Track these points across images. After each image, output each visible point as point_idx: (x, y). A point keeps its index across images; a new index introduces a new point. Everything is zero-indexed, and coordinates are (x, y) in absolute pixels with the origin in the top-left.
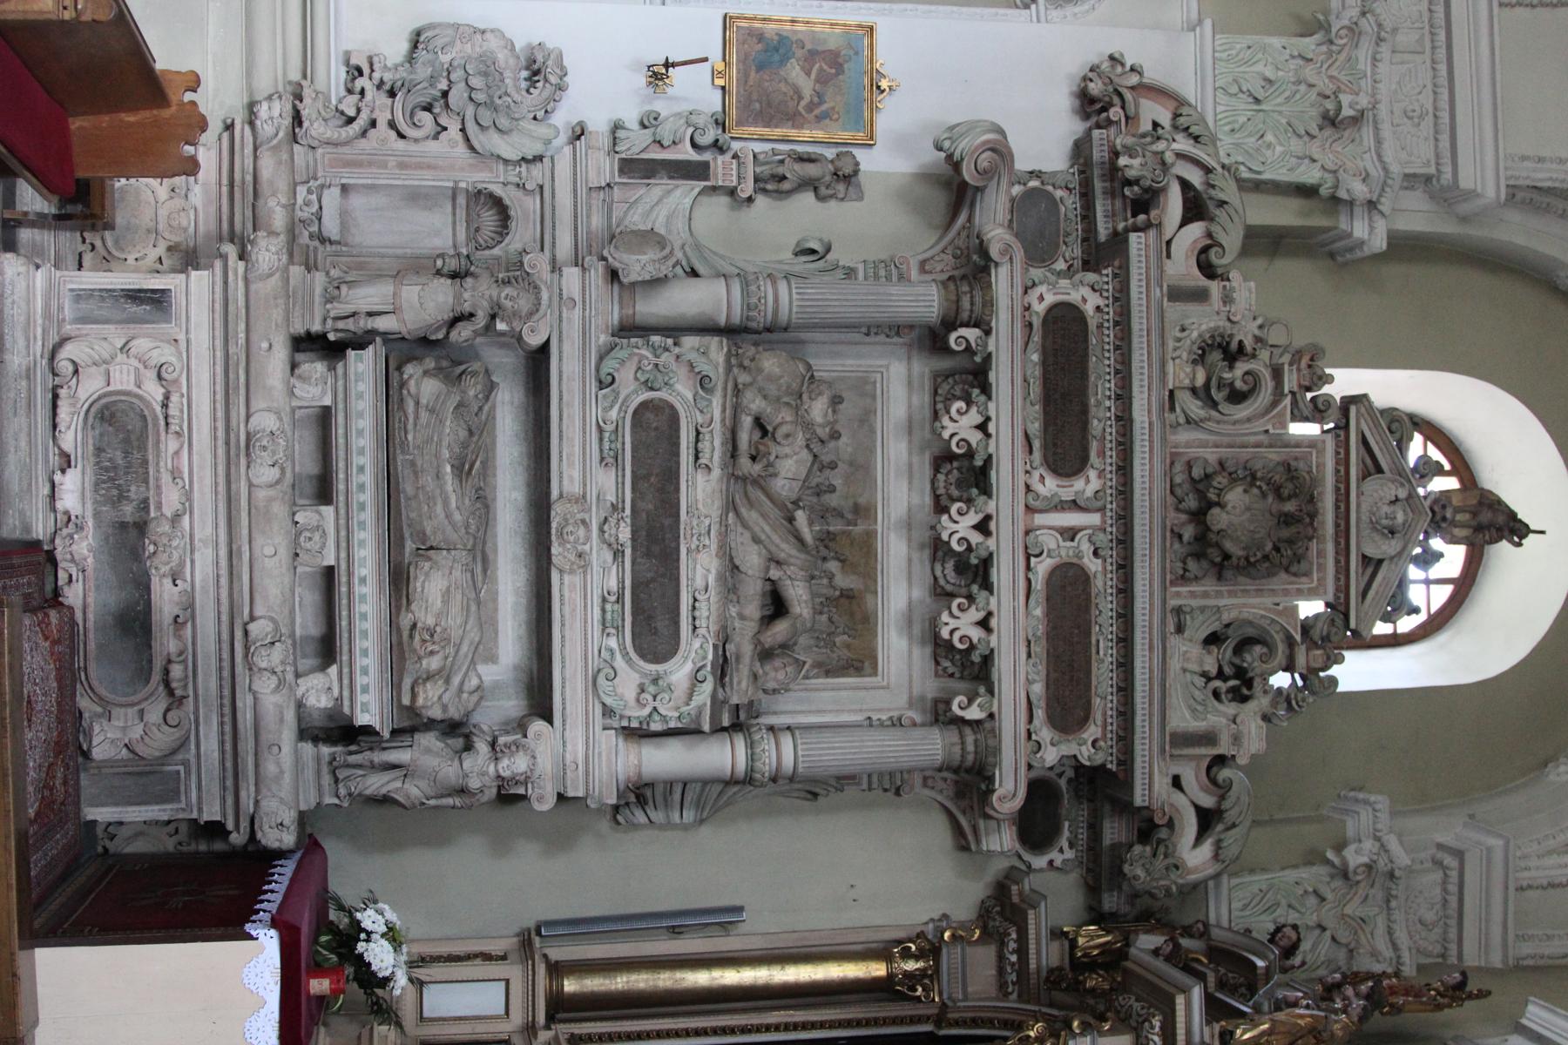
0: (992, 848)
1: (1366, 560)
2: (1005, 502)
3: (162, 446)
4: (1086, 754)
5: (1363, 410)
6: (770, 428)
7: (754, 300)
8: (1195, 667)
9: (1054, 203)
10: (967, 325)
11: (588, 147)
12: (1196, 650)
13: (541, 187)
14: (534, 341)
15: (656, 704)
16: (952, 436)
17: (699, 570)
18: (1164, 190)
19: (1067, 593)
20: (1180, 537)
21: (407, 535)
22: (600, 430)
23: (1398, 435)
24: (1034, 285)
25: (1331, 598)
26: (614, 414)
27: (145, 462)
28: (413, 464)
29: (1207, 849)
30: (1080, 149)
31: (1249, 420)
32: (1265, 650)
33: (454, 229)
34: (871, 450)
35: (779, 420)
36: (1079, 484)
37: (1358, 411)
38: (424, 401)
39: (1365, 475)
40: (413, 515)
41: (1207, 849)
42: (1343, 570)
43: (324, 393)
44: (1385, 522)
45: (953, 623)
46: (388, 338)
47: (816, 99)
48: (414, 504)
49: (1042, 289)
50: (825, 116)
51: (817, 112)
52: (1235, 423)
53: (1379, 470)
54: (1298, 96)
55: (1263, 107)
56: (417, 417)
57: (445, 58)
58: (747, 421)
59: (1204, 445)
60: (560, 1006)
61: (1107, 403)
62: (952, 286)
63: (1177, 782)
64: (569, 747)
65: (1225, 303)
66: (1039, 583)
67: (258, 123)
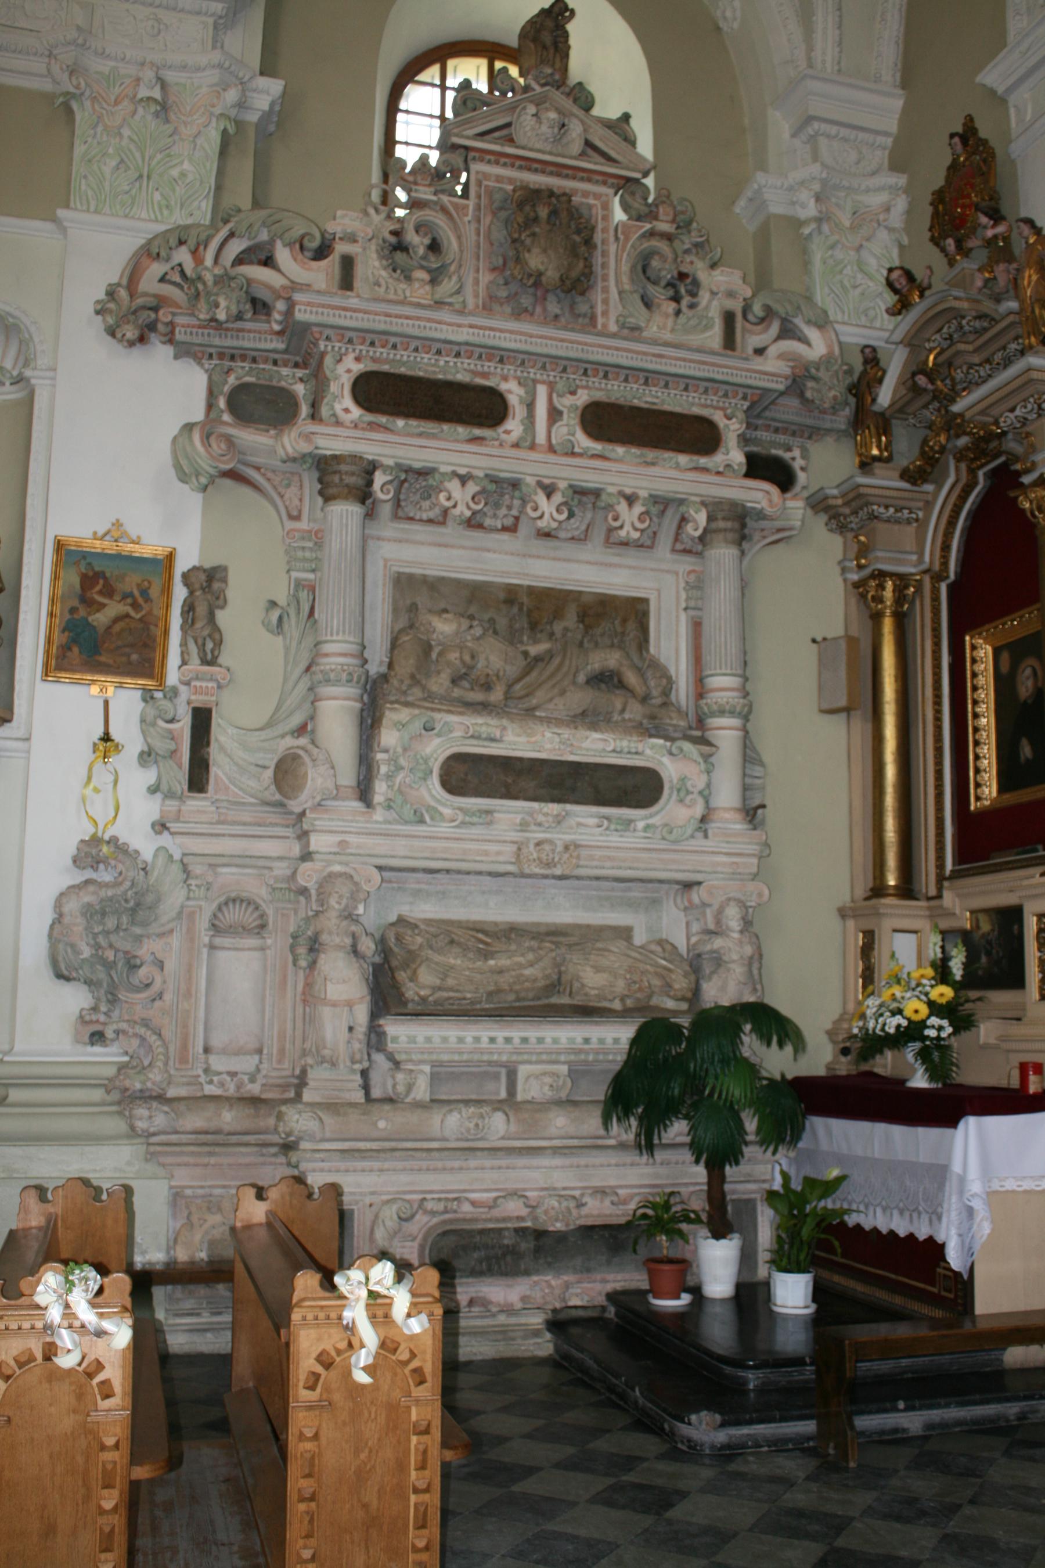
0: (800, 517)
1: (583, 154)
2: (530, 467)
3: (469, 1216)
4: (737, 426)
5: (455, 131)
6: (463, 671)
7: (344, 676)
8: (670, 322)
9: (242, 389)
10: (370, 483)
11: (177, 820)
12: (657, 319)
13: (210, 865)
14: (376, 876)
15: (696, 791)
16: (469, 508)
17: (596, 747)
18: (249, 282)
19: (607, 422)
20: (556, 316)
21: (545, 1001)
22: (463, 824)
23: (478, 104)
24: (334, 415)
25: (611, 191)
26: (447, 811)
27: (482, 1232)
28: (490, 994)
29: (813, 334)
30: (184, 351)
31: (459, 237)
32: (656, 257)
33: (243, 949)
34: (458, 582)
35: (457, 662)
36: (513, 400)
37: (457, 135)
38: (438, 982)
39: (511, 140)
40: (531, 995)
41: (813, 334)
42: (588, 176)
43: (422, 1072)
44: (556, 130)
45: (627, 527)
46: (375, 1015)
47: (129, 601)
48: (523, 994)
49: (338, 407)
50: (144, 593)
51: (140, 600)
52: (461, 251)
53: (508, 125)
54: (135, 138)
55: (145, 174)
56: (451, 989)
57: (86, 952)
58: (457, 692)
59: (476, 282)
60: (907, 890)
61: (442, 363)
62: (331, 491)
63: (760, 351)
64: (719, 869)
65: (355, 241)
66: (597, 447)
67: (152, 1130)
